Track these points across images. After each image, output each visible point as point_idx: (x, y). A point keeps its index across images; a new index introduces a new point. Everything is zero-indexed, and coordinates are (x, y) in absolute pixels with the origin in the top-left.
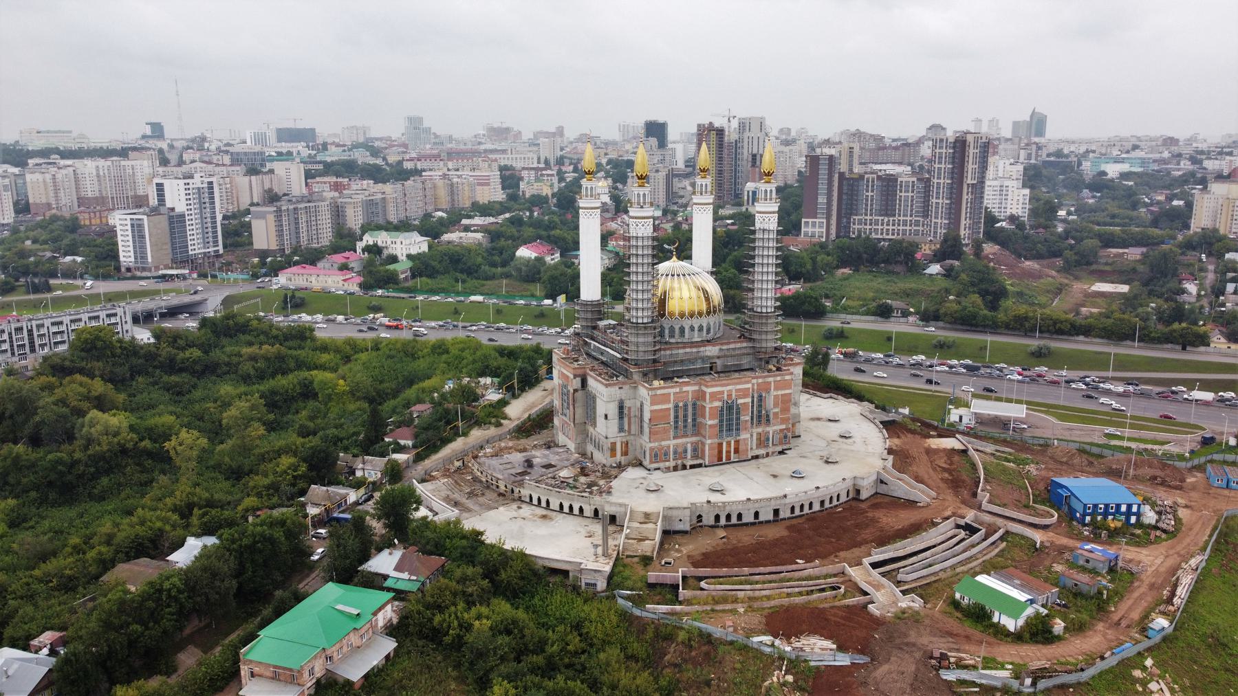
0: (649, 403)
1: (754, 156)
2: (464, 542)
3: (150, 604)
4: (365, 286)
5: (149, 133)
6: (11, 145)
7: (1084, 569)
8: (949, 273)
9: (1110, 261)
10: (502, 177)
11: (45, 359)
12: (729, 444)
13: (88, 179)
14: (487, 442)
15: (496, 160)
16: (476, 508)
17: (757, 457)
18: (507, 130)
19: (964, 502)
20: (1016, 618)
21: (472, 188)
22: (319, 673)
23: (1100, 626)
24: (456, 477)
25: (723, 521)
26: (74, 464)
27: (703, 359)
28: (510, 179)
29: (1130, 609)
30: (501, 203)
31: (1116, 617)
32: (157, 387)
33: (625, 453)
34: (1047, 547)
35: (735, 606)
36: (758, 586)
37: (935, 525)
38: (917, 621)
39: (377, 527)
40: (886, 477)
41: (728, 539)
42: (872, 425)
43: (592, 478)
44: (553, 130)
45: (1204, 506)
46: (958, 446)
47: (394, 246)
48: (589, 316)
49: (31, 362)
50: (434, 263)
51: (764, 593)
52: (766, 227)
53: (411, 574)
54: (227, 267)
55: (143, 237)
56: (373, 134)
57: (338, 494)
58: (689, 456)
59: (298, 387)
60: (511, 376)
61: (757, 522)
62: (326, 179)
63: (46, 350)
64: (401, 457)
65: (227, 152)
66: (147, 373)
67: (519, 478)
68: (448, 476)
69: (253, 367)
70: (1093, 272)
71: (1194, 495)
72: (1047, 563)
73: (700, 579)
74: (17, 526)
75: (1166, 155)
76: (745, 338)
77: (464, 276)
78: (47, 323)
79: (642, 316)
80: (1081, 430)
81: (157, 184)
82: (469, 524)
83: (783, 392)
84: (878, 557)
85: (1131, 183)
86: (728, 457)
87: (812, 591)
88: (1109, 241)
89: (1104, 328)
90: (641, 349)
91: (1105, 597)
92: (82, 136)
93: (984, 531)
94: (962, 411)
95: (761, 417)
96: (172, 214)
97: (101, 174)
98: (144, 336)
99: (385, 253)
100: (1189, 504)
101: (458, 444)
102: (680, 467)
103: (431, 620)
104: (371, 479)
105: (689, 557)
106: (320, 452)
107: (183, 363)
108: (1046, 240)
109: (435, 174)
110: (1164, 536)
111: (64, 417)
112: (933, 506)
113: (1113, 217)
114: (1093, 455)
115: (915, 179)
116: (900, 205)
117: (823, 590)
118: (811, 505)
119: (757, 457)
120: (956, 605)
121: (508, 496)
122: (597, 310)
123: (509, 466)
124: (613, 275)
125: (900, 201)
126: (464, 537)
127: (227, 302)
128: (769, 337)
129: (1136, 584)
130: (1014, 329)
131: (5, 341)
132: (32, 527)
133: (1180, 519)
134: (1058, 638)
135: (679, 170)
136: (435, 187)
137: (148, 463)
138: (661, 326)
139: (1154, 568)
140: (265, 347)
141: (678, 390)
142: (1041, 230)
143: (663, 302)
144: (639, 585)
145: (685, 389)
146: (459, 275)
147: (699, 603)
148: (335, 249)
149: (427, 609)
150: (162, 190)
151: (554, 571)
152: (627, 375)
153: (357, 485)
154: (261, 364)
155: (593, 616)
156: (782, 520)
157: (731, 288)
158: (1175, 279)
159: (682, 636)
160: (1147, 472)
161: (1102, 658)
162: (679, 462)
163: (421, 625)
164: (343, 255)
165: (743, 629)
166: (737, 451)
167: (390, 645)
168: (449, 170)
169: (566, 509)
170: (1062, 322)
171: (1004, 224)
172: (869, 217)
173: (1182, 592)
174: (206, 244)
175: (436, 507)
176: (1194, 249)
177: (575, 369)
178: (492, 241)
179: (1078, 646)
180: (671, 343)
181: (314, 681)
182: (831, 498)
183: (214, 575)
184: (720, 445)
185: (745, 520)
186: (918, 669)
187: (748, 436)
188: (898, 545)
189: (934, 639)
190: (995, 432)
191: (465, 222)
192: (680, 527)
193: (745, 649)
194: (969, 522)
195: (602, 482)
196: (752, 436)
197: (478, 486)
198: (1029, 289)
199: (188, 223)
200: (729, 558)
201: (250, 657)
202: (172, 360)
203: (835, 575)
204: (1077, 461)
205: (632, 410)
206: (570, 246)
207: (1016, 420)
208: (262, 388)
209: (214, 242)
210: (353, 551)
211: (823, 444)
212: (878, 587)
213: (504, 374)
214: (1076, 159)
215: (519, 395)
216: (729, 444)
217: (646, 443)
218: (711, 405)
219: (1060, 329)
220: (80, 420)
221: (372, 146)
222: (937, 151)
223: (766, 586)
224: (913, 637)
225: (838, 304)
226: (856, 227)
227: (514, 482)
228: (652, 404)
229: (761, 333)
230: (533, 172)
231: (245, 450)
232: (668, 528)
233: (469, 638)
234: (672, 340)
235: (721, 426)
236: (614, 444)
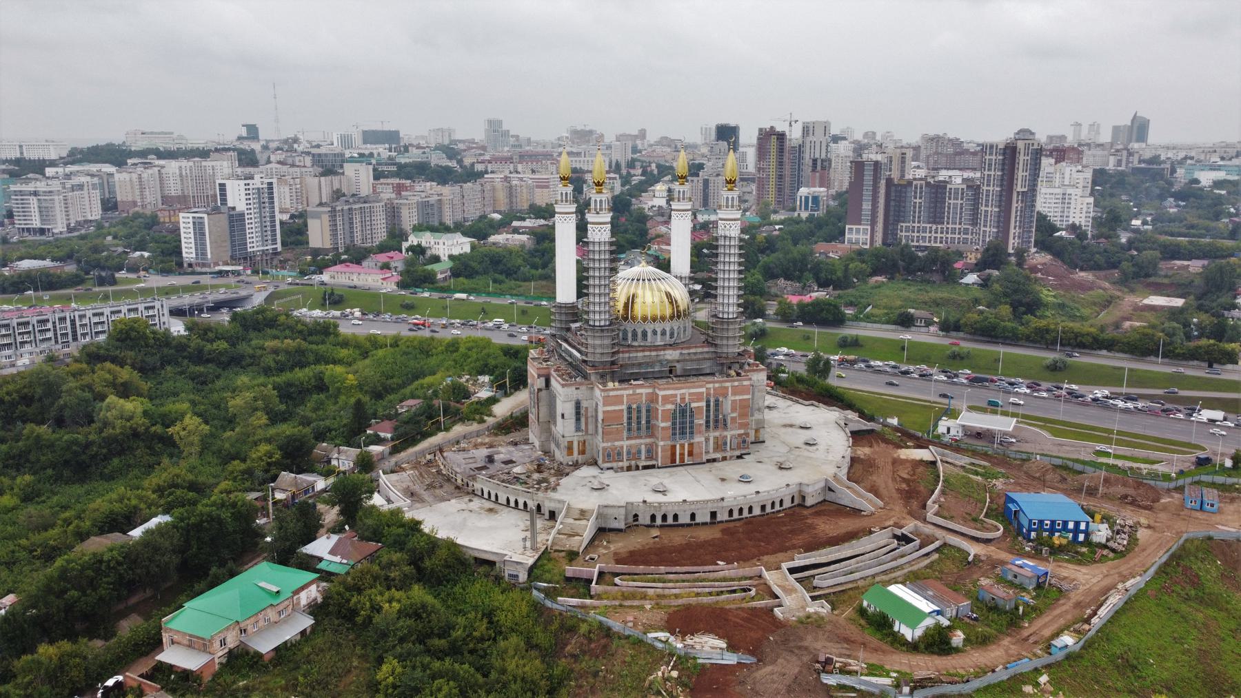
2: (401, 530)
3: (90, 573)
4: (402, 285)
5: (244, 134)
6: (119, 145)
8: (985, 283)
11: (85, 347)
12: (682, 446)
13: (171, 178)
17: (714, 460)
18: (591, 132)
20: (913, 627)
21: (531, 190)
22: (232, 642)
23: (1006, 641)
25: (659, 521)
26: (89, 445)
29: (1045, 626)
31: (1025, 633)
33: (582, 452)
34: (982, 561)
35: (642, 602)
38: (819, 626)
40: (834, 484)
44: (636, 133)
45: (1168, 527)
47: (437, 246)
48: (563, 318)
49: (74, 349)
50: (473, 264)
51: (674, 591)
53: (342, 558)
54: (283, 265)
55: (204, 234)
58: (643, 457)
59: (313, 380)
60: (503, 375)
62: (389, 181)
63: (88, 339)
64: (375, 449)
66: (177, 363)
69: (274, 359)
70: (1149, 285)
71: (1163, 516)
72: (975, 577)
73: (617, 575)
74: (31, 500)
76: (708, 343)
77: (502, 277)
78: (89, 314)
80: (1072, 446)
82: (411, 513)
83: (741, 397)
84: (798, 563)
85: (1223, 192)
86: (682, 460)
87: (722, 592)
88: (1173, 253)
92: (181, 137)
93: (918, 542)
95: (716, 420)
96: (232, 213)
97: (184, 174)
98: (177, 328)
99: (429, 253)
100: (1152, 523)
102: (634, 467)
103: (348, 601)
104: (342, 469)
106: (295, 440)
108: (1105, 251)
110: (1111, 555)
111: (86, 401)
113: (1192, 227)
115: (964, 186)
116: (949, 213)
117: (734, 591)
119: (714, 460)
120: (862, 612)
121: (463, 490)
122: (573, 313)
123: (471, 461)
125: (949, 208)
126: (403, 525)
127: (270, 299)
128: (731, 342)
129: (1061, 602)
130: (1034, 341)
131: (49, 330)
132: (44, 502)
134: (957, 650)
135: (749, 173)
136: (494, 189)
137: (158, 446)
140: (288, 341)
141: (631, 392)
142: (1102, 240)
147: (608, 598)
148: (383, 249)
150: (225, 190)
154: (281, 358)
156: (719, 522)
157: (753, 293)
158: (1230, 294)
159: (584, 628)
160: (1120, 490)
161: (993, 671)
162: (633, 463)
163: (340, 605)
164: (388, 254)
166: (691, 454)
167: (307, 622)
169: (512, 504)
170: (1083, 335)
171: (1063, 233)
173: (1104, 612)
174: (264, 241)
178: (538, 243)
179: (974, 659)
180: (633, 346)
181: (227, 650)
183: (156, 549)
184: (674, 447)
185: (681, 521)
186: (800, 672)
188: (824, 551)
189: (829, 644)
190: (979, 445)
191: (515, 224)
192: (615, 525)
193: (639, 643)
194: (905, 533)
197: (440, 478)
199: (247, 221)
201: (172, 625)
202: (200, 351)
203: (751, 578)
205: (590, 410)
207: (1005, 434)
208: (277, 379)
209: (273, 240)
211: (784, 450)
212: (789, 591)
215: (511, 394)
216: (682, 446)
219: (1081, 342)
220: (100, 404)
224: (809, 641)
226: (904, 234)
228: (604, 405)
229: (722, 338)
232: (603, 526)
233: (377, 619)
234: (635, 344)
235: (674, 429)
236: (570, 444)
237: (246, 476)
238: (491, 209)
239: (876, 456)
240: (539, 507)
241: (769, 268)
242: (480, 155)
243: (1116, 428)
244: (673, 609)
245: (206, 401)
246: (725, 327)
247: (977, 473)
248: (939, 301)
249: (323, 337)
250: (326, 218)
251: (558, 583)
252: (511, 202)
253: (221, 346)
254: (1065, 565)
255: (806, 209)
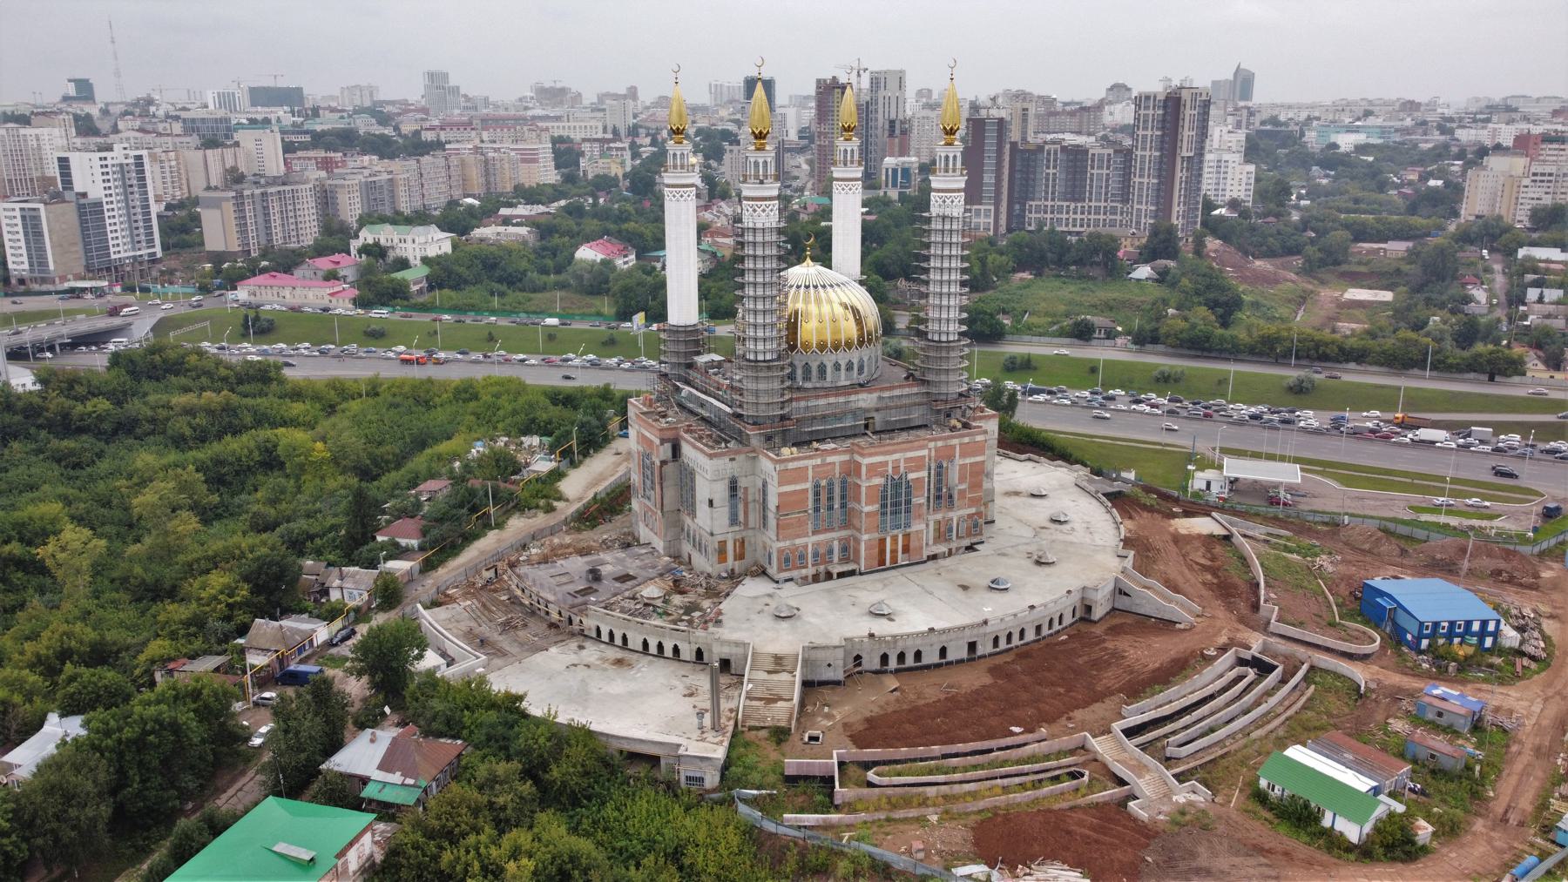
0: (776, 483)
1: (892, 123)
7: (1436, 728)
8: (1162, 277)
9: (1366, 259)
10: (555, 151)
12: (895, 539)
14: (533, 538)
15: (547, 129)
16: (514, 649)
17: (934, 557)
18: (563, 91)
19: (1242, 620)
23: (1479, 825)
24: (485, 597)
25: (893, 664)
27: (855, 413)
28: (566, 154)
30: (553, 186)
31: (1498, 807)
32: (41, 456)
33: (740, 556)
34: (1373, 691)
36: (957, 776)
37: (1209, 660)
39: (355, 688)
40: (1130, 584)
41: (903, 691)
42: (1094, 502)
43: (691, 597)
44: (623, 91)
46: (1219, 531)
47: (402, 245)
48: (682, 348)
50: (461, 270)
51: (967, 787)
52: (948, 212)
53: (405, 775)
54: (168, 276)
55: (40, 234)
56: (381, 96)
57: (298, 631)
58: (836, 559)
59: (256, 454)
61: (944, 663)
62: (311, 154)
64: (399, 566)
65: (177, 118)
66: (28, 437)
67: (580, 599)
68: (474, 595)
69: (189, 424)
70: (1343, 275)
72: (1379, 717)
73: (867, 766)
75: (1408, 122)
76: (915, 379)
77: (504, 288)
79: (764, 349)
80: (1377, 499)
81: (60, 159)
82: (501, 682)
83: (973, 460)
85: (1371, 159)
86: (894, 559)
87: (1040, 781)
88: (1361, 234)
89: (1384, 352)
90: (762, 400)
91: (1477, 773)
94: (1210, 474)
95: (942, 497)
96: (83, 201)
99: (391, 255)
101: (489, 542)
102: (822, 576)
103: (435, 858)
104: (351, 604)
105: (845, 725)
106: (271, 564)
107: (82, 420)
108: (1279, 233)
109: (463, 145)
110: (1534, 666)
112: (1199, 628)
113: (1357, 201)
114: (1401, 537)
115: (1111, 151)
116: (1091, 187)
117: (1056, 779)
118: (1022, 633)
119: (934, 557)
120: (1261, 797)
121: (563, 629)
122: (693, 340)
123: (564, 579)
124: (710, 283)
125: (1092, 180)
126: (493, 705)
127: (160, 327)
128: (952, 378)
129: (1514, 748)
130: (1261, 354)
133: (1549, 638)
134: (1425, 850)
136: (463, 164)
137: (17, 577)
138: (791, 365)
139: (1533, 721)
141: (819, 461)
142: (1271, 219)
143: (793, 326)
144: (772, 778)
145: (830, 459)
146: (496, 286)
147: (867, 810)
148: (320, 250)
149: (431, 838)
150: (68, 167)
151: (634, 757)
152: (742, 439)
153: (330, 615)
154: (201, 420)
155: (701, 837)
156: (980, 657)
160: (1487, 564)
162: (822, 568)
164: (333, 258)
165: (939, 852)
166: (906, 549)
168: (482, 141)
169: (653, 649)
170: (1326, 344)
171: (1223, 211)
172: (1049, 203)
174: (135, 244)
175: (452, 650)
176: (1472, 243)
177: (661, 430)
178: (542, 238)
180: (806, 390)
182: (1051, 621)
183: (69, 798)
184: (882, 541)
185: (926, 660)
187: (923, 526)
188: (1160, 697)
189: (1237, 860)
191: (504, 211)
192: (829, 675)
195: (706, 604)
196: (927, 525)
198: (1266, 298)
200: (907, 726)
203: (1072, 752)
204: (1385, 548)
205: (751, 491)
206: (650, 243)
210: (311, 737)
211: (1028, 533)
212: (1140, 769)
213: (557, 433)
214: (1297, 128)
215: (581, 462)
216: (895, 539)
217: (772, 542)
218: (869, 483)
221: (381, 112)
222: (1142, 112)
223: (970, 775)
225: (1019, 322)
226: (1033, 215)
227: (573, 606)
228: (781, 484)
229: (939, 372)
230: (596, 145)
231: (167, 553)
232: (810, 678)
234: (808, 385)
236: (723, 544)
237: (193, 629)
238: (460, 192)
239: (1146, 533)
240: (699, 653)
241: (884, 265)
242: (422, 120)
243: (1450, 473)
244: (973, 817)
245: (83, 495)
246: (944, 354)
247: (1291, 552)
248: (1112, 303)
249: (260, 385)
250: (229, 207)
251: (773, 787)
252: (488, 183)
253: (100, 406)
254: (1484, 686)
255: (895, 185)
